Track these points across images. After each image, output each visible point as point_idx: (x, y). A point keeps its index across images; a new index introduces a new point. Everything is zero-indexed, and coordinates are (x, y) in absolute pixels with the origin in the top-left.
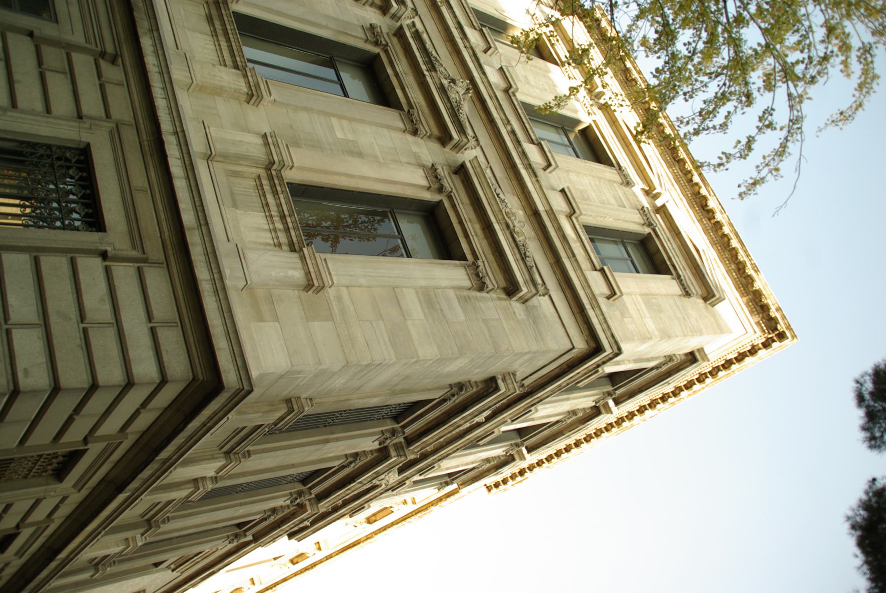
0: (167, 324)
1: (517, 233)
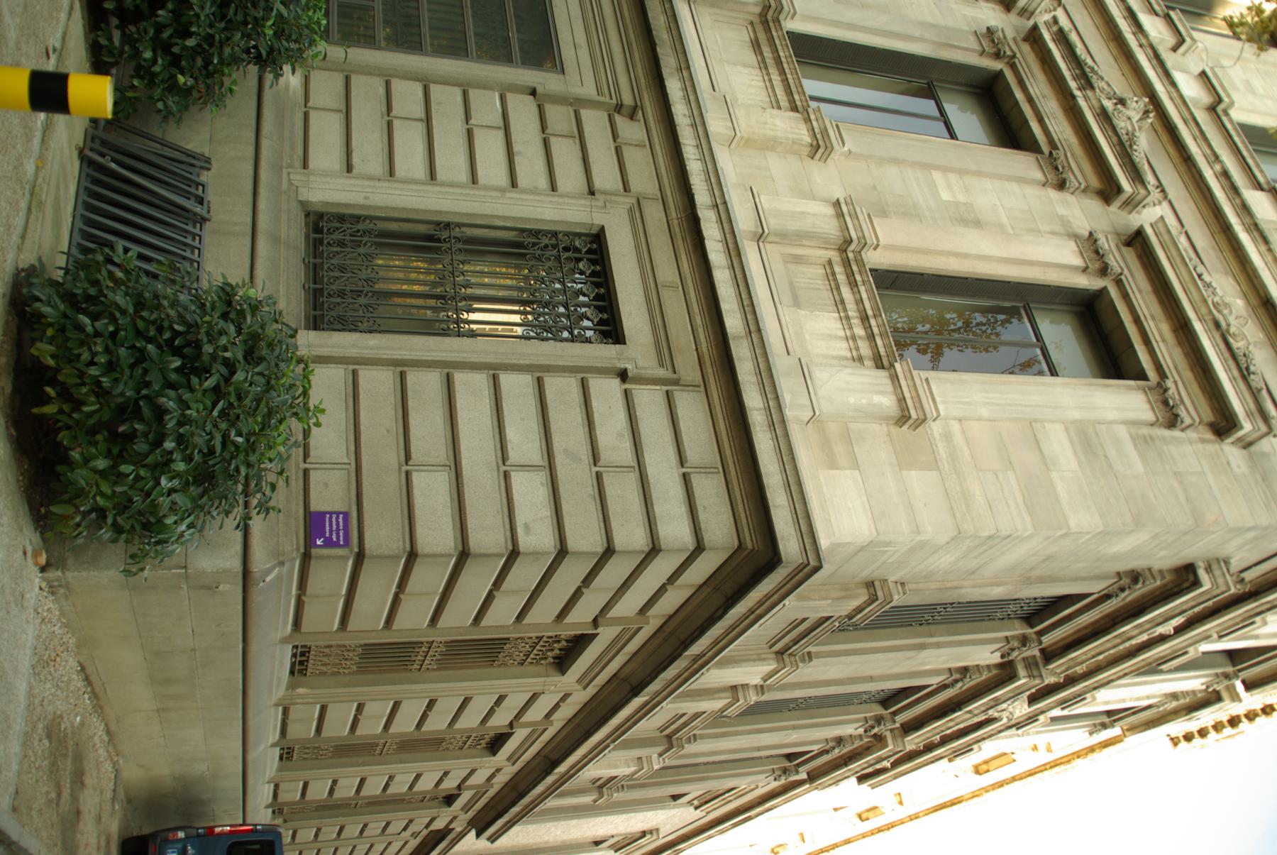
0: (705, 469)
1: (1234, 336)
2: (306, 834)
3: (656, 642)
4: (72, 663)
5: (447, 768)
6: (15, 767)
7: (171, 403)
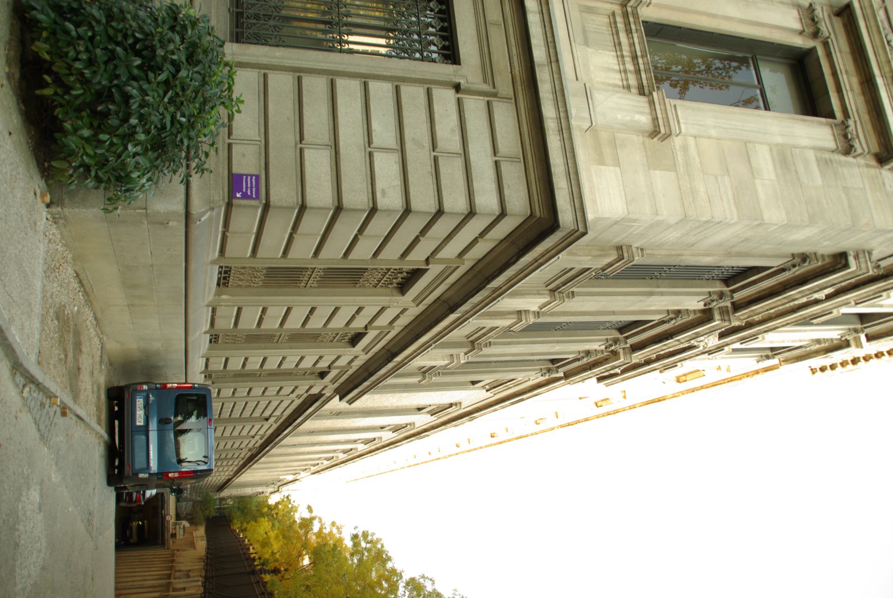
0: (511, 159)
2: (227, 392)
3: (468, 277)
4: (70, 271)
5: (321, 354)
6: (37, 336)
7: (135, 91)
